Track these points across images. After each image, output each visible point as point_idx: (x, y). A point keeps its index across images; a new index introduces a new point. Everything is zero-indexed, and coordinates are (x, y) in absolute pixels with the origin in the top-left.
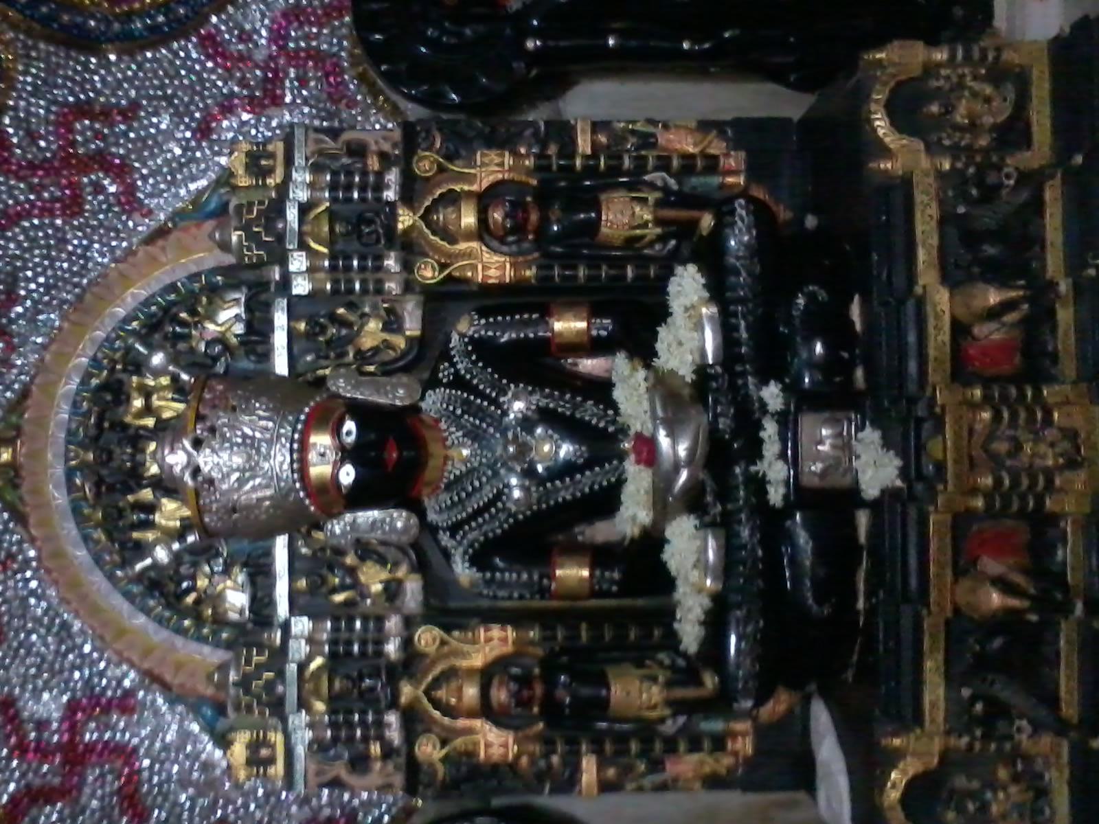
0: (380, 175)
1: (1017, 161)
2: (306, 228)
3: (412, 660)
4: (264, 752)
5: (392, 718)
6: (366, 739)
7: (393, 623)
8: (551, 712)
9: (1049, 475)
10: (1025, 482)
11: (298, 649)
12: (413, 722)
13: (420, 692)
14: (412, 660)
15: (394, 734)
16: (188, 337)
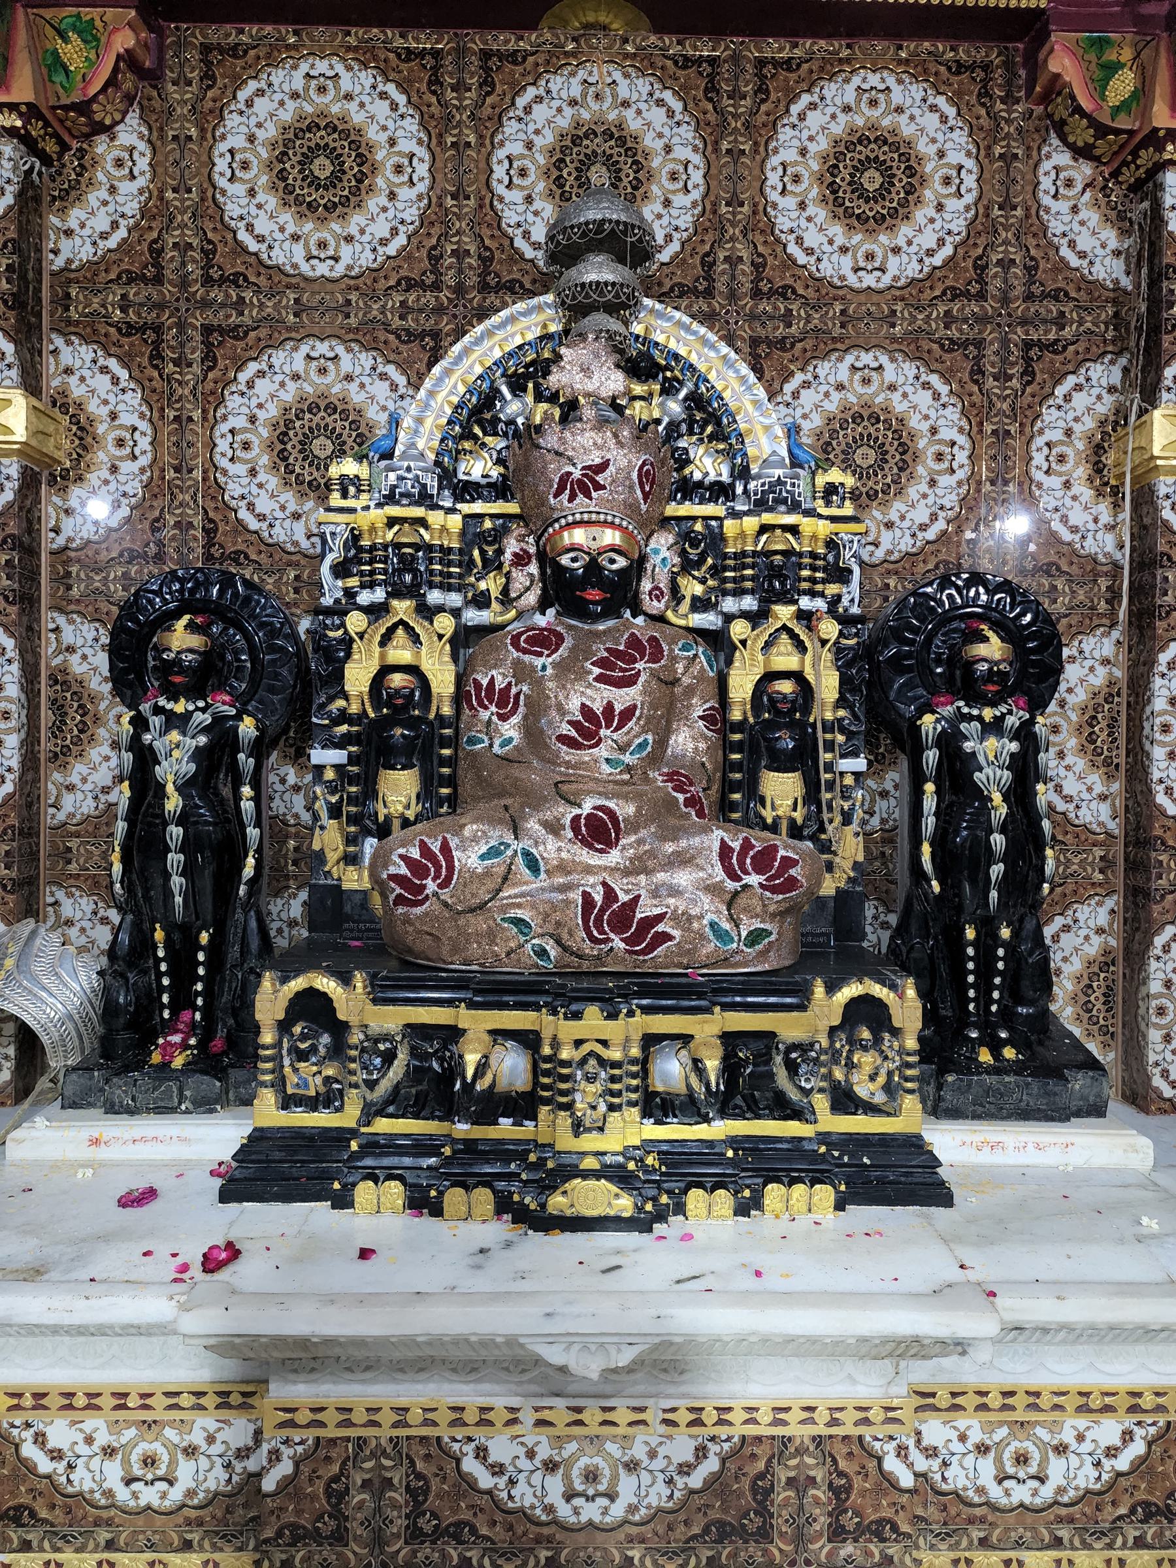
0: (822, 594)
1: (821, 1103)
2: (778, 532)
3: (427, 612)
4: (352, 490)
5: (379, 594)
6: (362, 574)
7: (455, 599)
8: (384, 724)
9: (569, 1107)
10: (564, 1086)
11: (435, 518)
12: (375, 611)
13: (401, 616)
14: (427, 612)
15: (364, 598)
16: (691, 432)
